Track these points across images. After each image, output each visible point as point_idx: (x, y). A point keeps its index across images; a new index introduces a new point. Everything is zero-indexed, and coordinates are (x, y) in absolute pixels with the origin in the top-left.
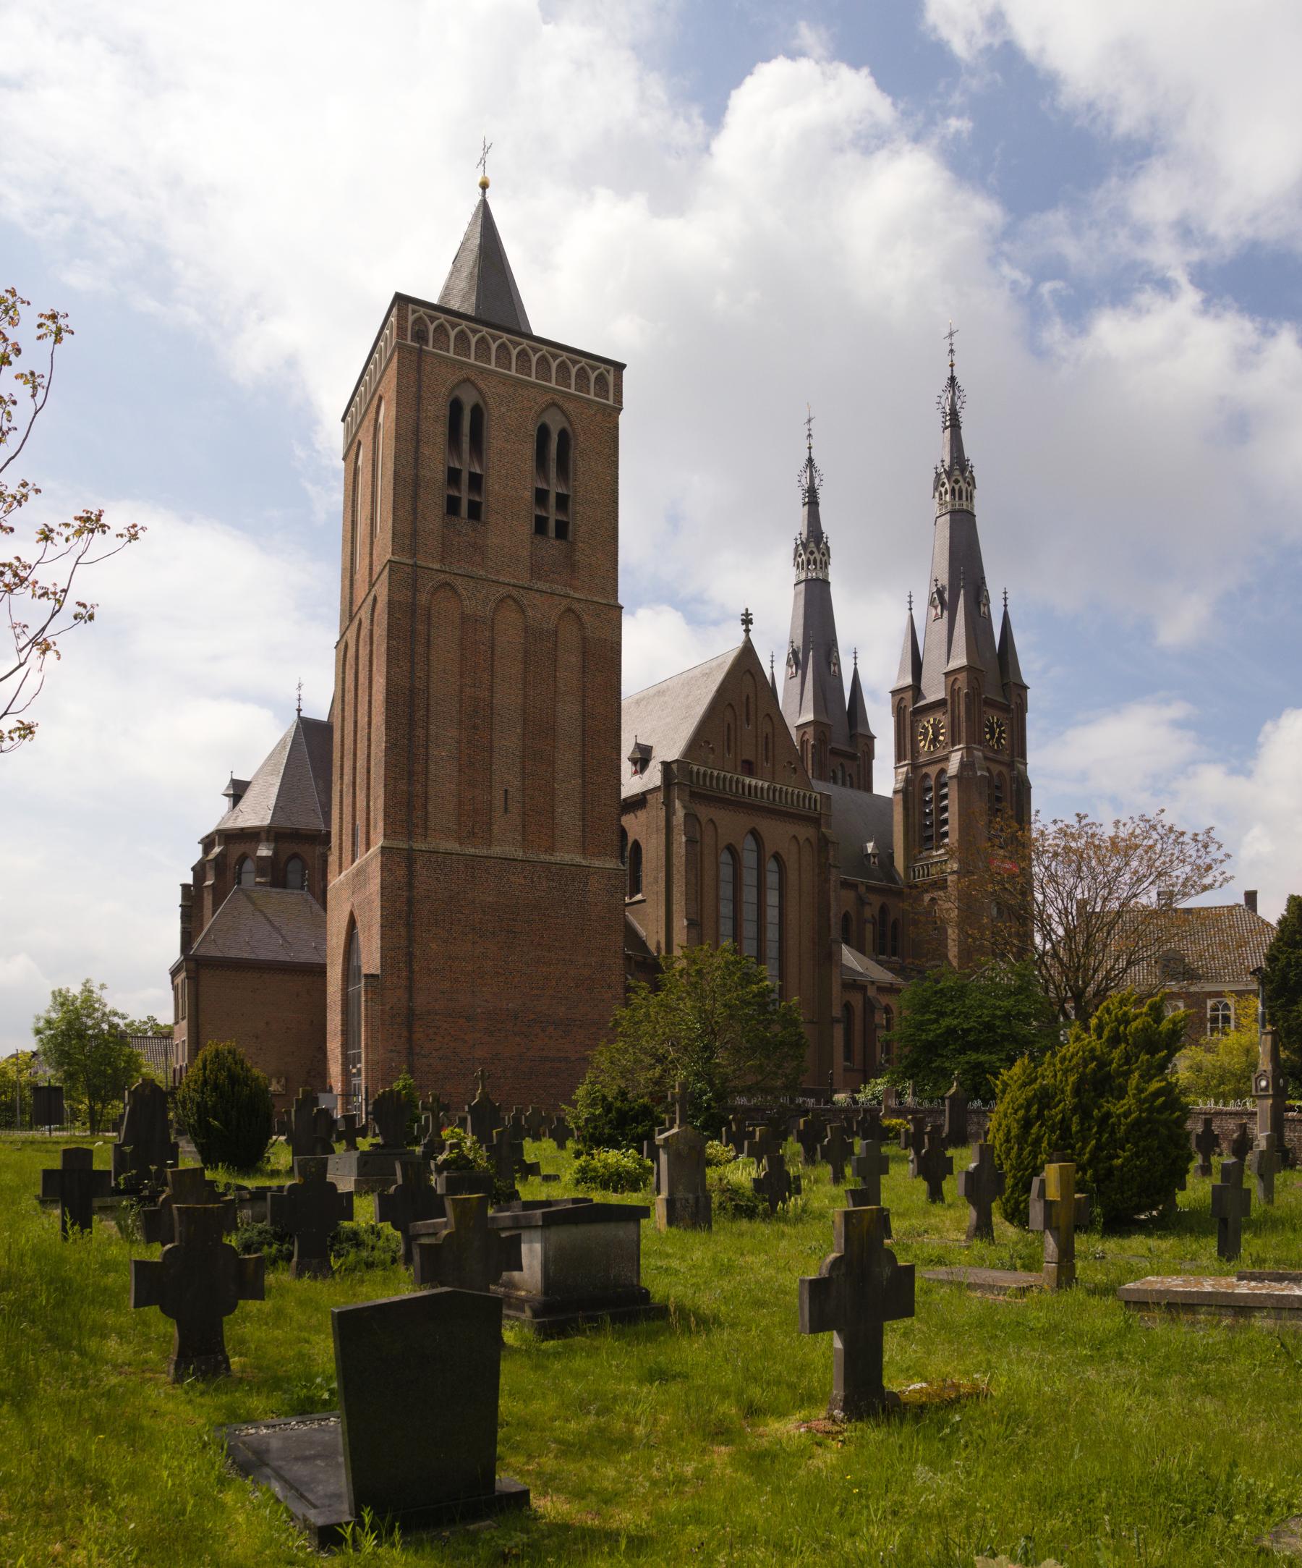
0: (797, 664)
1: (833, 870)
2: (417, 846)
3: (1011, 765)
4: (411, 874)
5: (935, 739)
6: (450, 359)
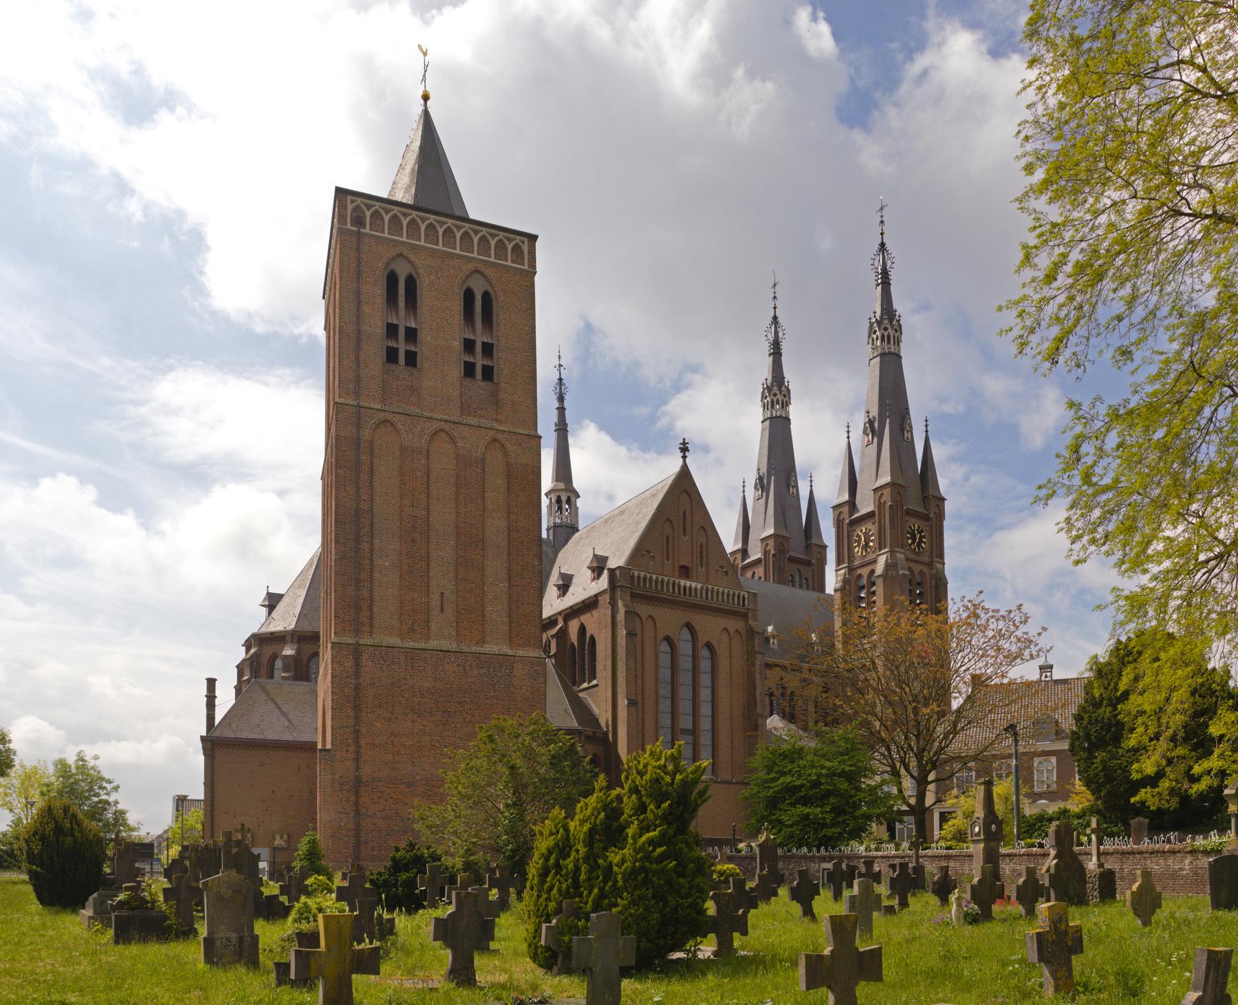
0: (762, 488)
1: (759, 656)
2: (362, 642)
3: (930, 565)
4: (358, 664)
5: (867, 545)
6: (385, 238)
